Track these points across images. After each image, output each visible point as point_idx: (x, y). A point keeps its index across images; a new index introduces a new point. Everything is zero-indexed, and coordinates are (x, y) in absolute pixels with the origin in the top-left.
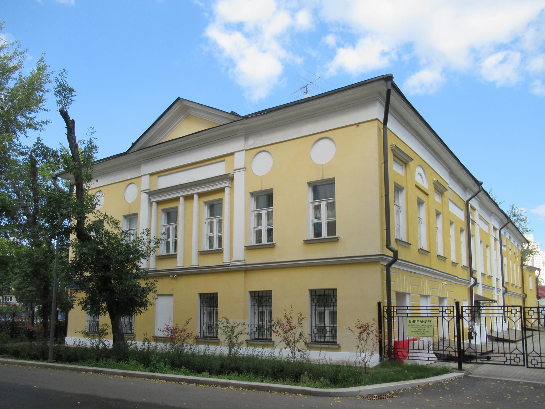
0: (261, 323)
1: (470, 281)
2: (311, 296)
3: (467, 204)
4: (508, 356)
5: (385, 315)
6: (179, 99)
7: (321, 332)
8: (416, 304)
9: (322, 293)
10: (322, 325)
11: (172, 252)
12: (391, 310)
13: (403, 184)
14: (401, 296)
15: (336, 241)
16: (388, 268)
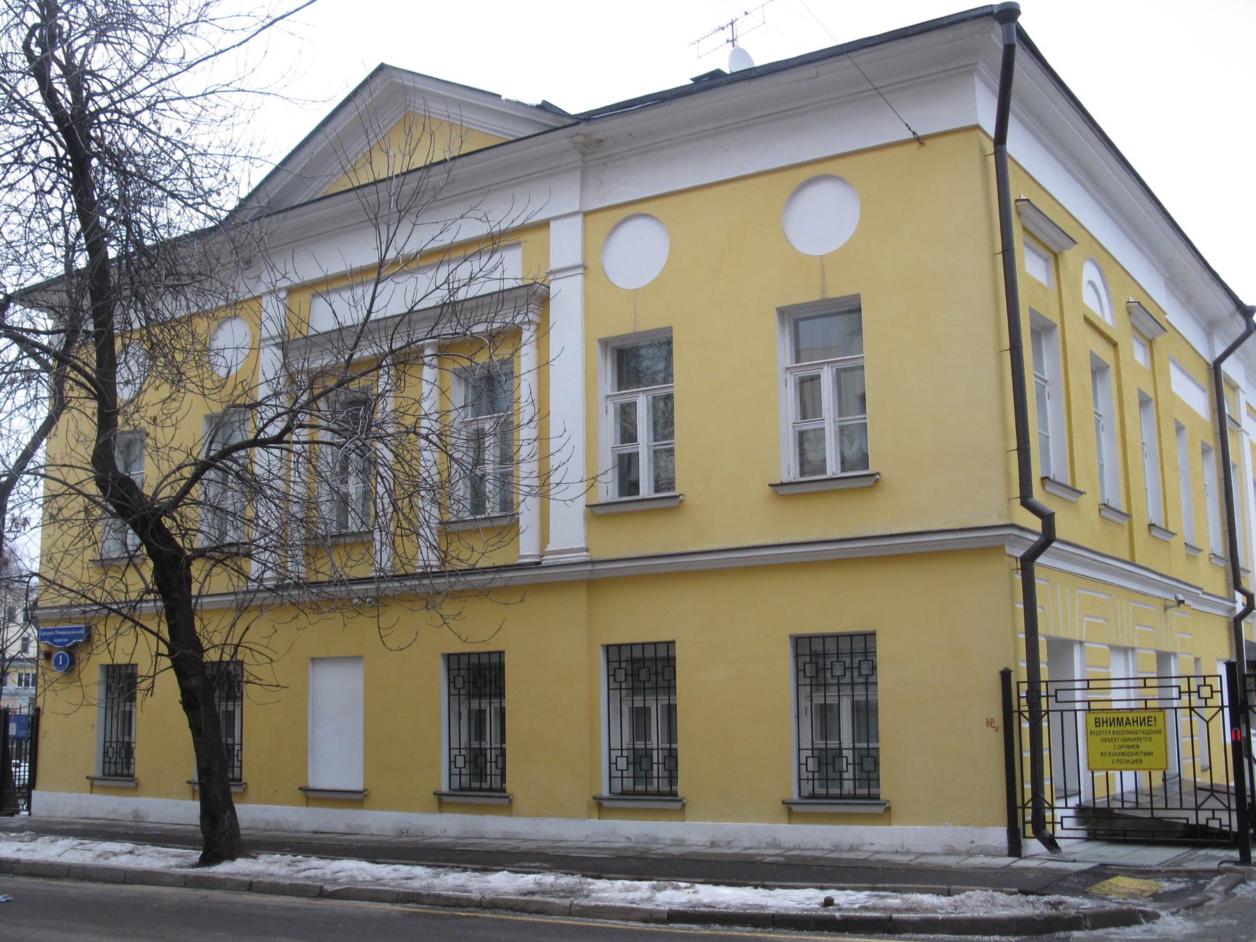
0: (640, 745)
1: (1235, 602)
2: (797, 656)
3: (1215, 369)
5: (1022, 709)
6: (382, 67)
7: (830, 767)
8: (1100, 673)
9: (649, 653)
10: (833, 744)
11: (353, 525)
12: (1039, 691)
13: (1053, 317)
14: (1062, 648)
15: (870, 487)
16: (1027, 563)
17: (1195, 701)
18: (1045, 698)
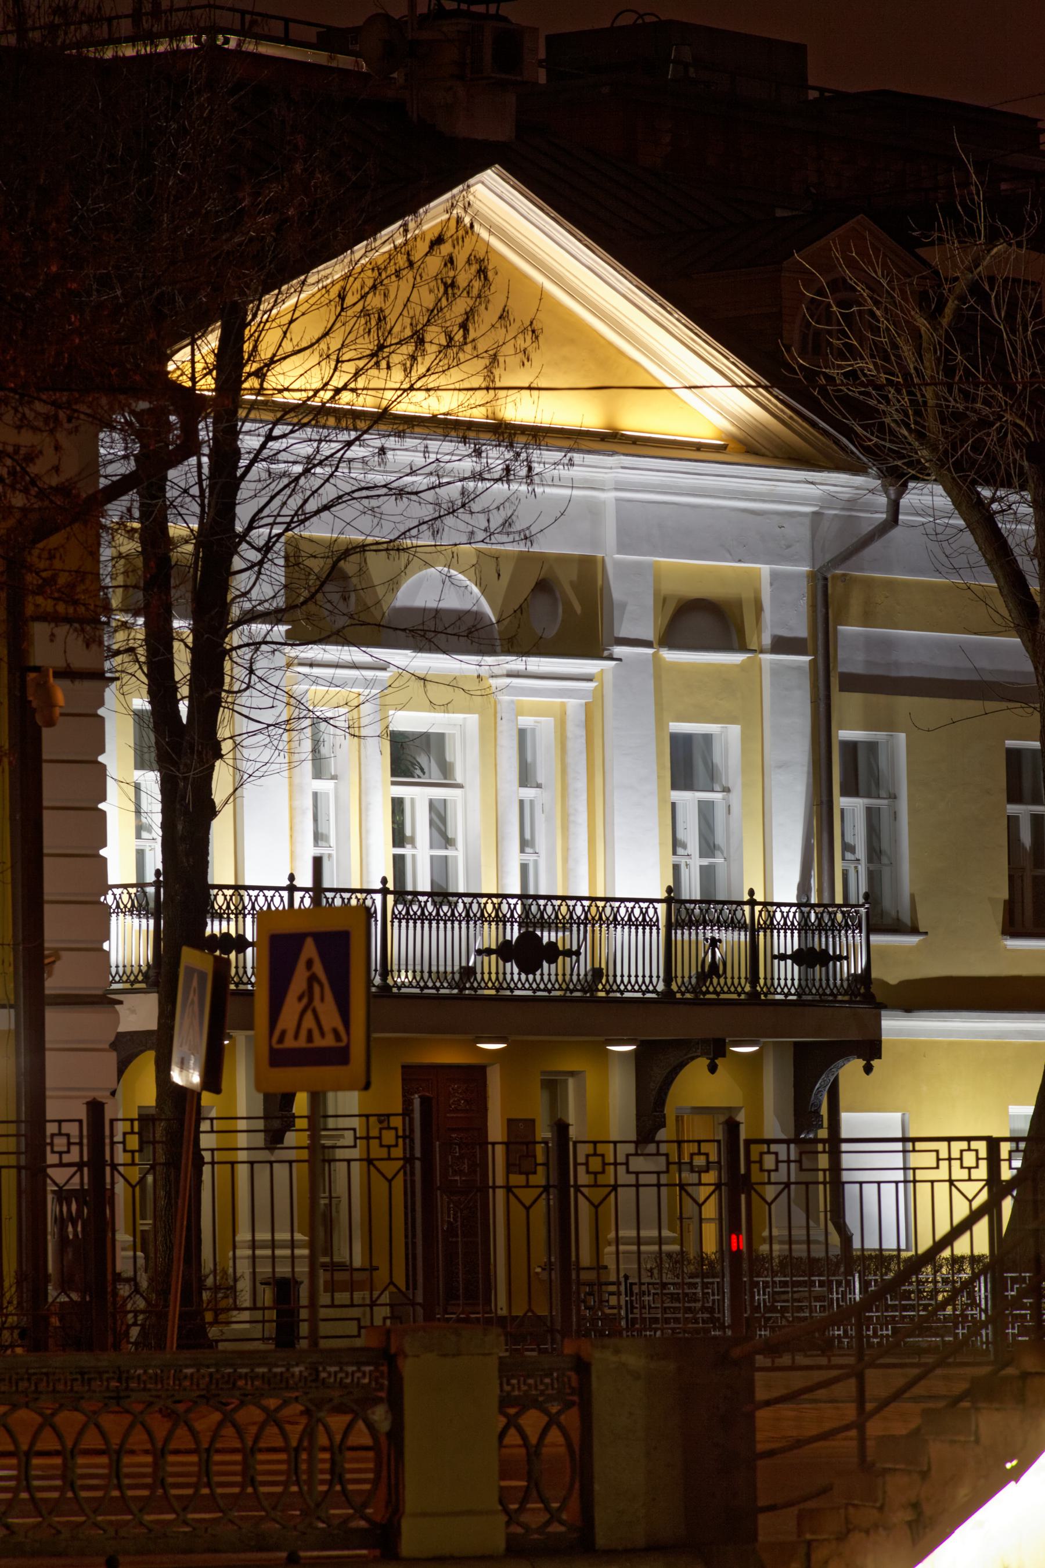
4: (624, 1178)
17: (958, 1173)
18: (655, 1182)
